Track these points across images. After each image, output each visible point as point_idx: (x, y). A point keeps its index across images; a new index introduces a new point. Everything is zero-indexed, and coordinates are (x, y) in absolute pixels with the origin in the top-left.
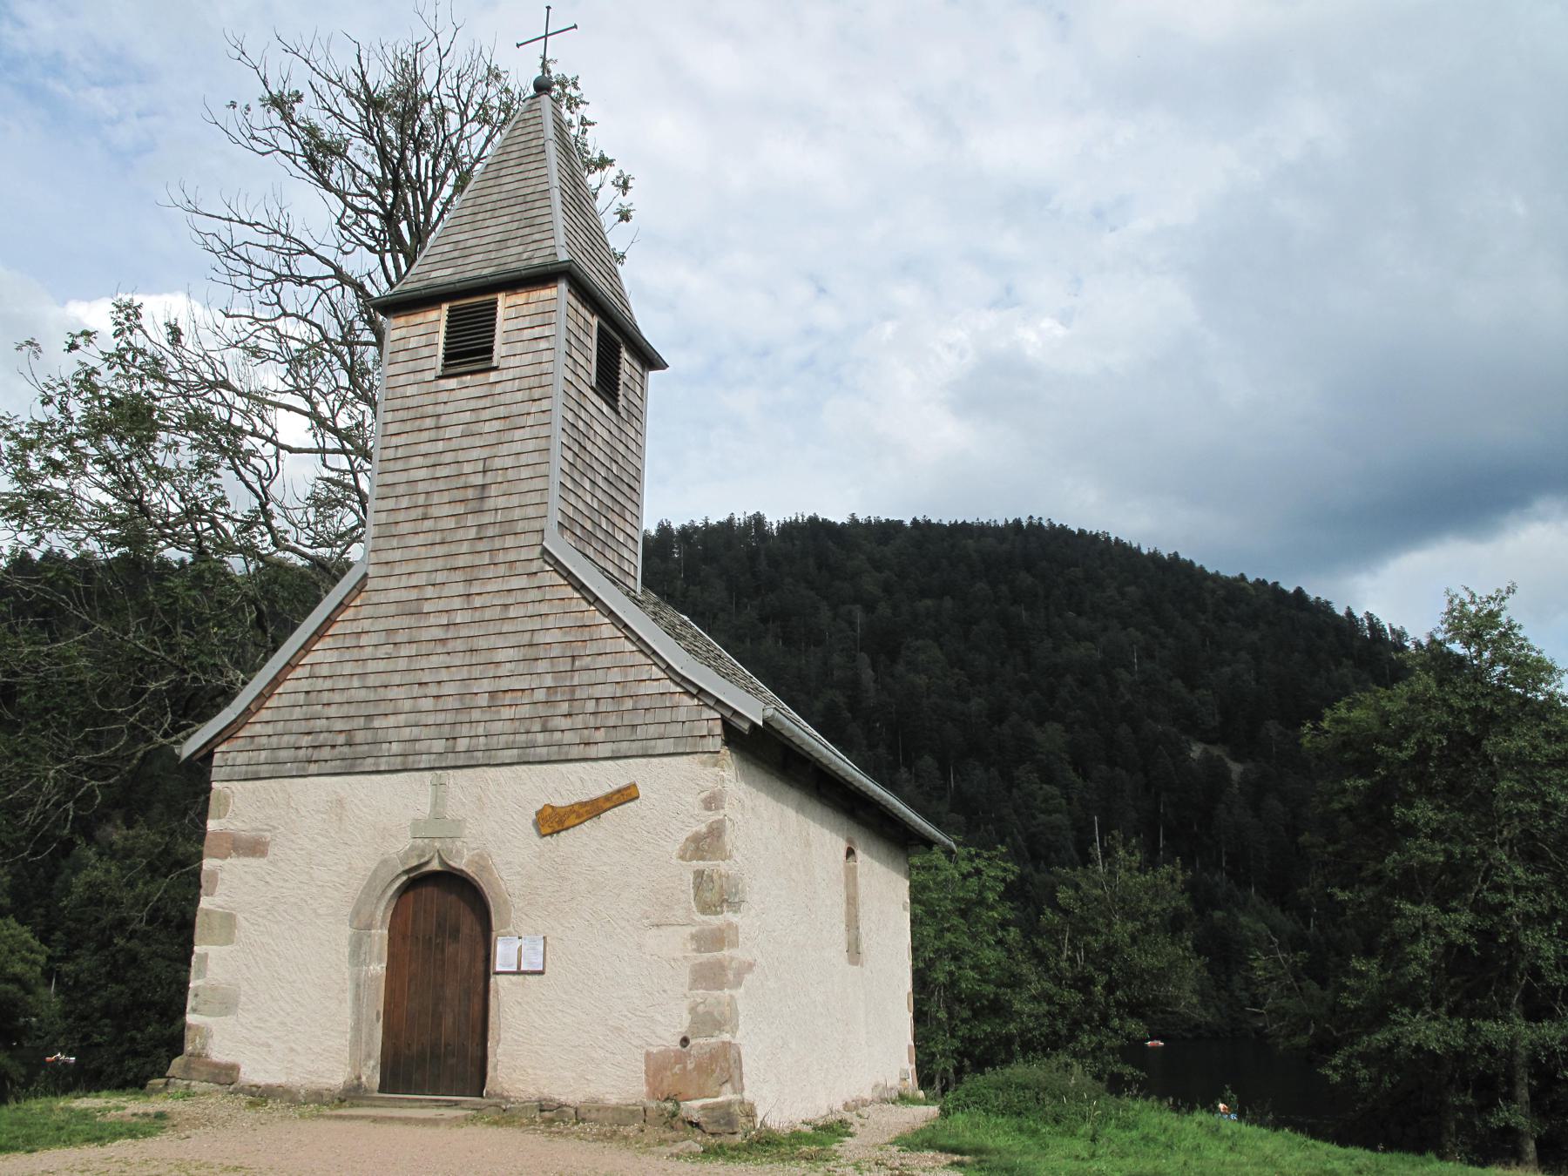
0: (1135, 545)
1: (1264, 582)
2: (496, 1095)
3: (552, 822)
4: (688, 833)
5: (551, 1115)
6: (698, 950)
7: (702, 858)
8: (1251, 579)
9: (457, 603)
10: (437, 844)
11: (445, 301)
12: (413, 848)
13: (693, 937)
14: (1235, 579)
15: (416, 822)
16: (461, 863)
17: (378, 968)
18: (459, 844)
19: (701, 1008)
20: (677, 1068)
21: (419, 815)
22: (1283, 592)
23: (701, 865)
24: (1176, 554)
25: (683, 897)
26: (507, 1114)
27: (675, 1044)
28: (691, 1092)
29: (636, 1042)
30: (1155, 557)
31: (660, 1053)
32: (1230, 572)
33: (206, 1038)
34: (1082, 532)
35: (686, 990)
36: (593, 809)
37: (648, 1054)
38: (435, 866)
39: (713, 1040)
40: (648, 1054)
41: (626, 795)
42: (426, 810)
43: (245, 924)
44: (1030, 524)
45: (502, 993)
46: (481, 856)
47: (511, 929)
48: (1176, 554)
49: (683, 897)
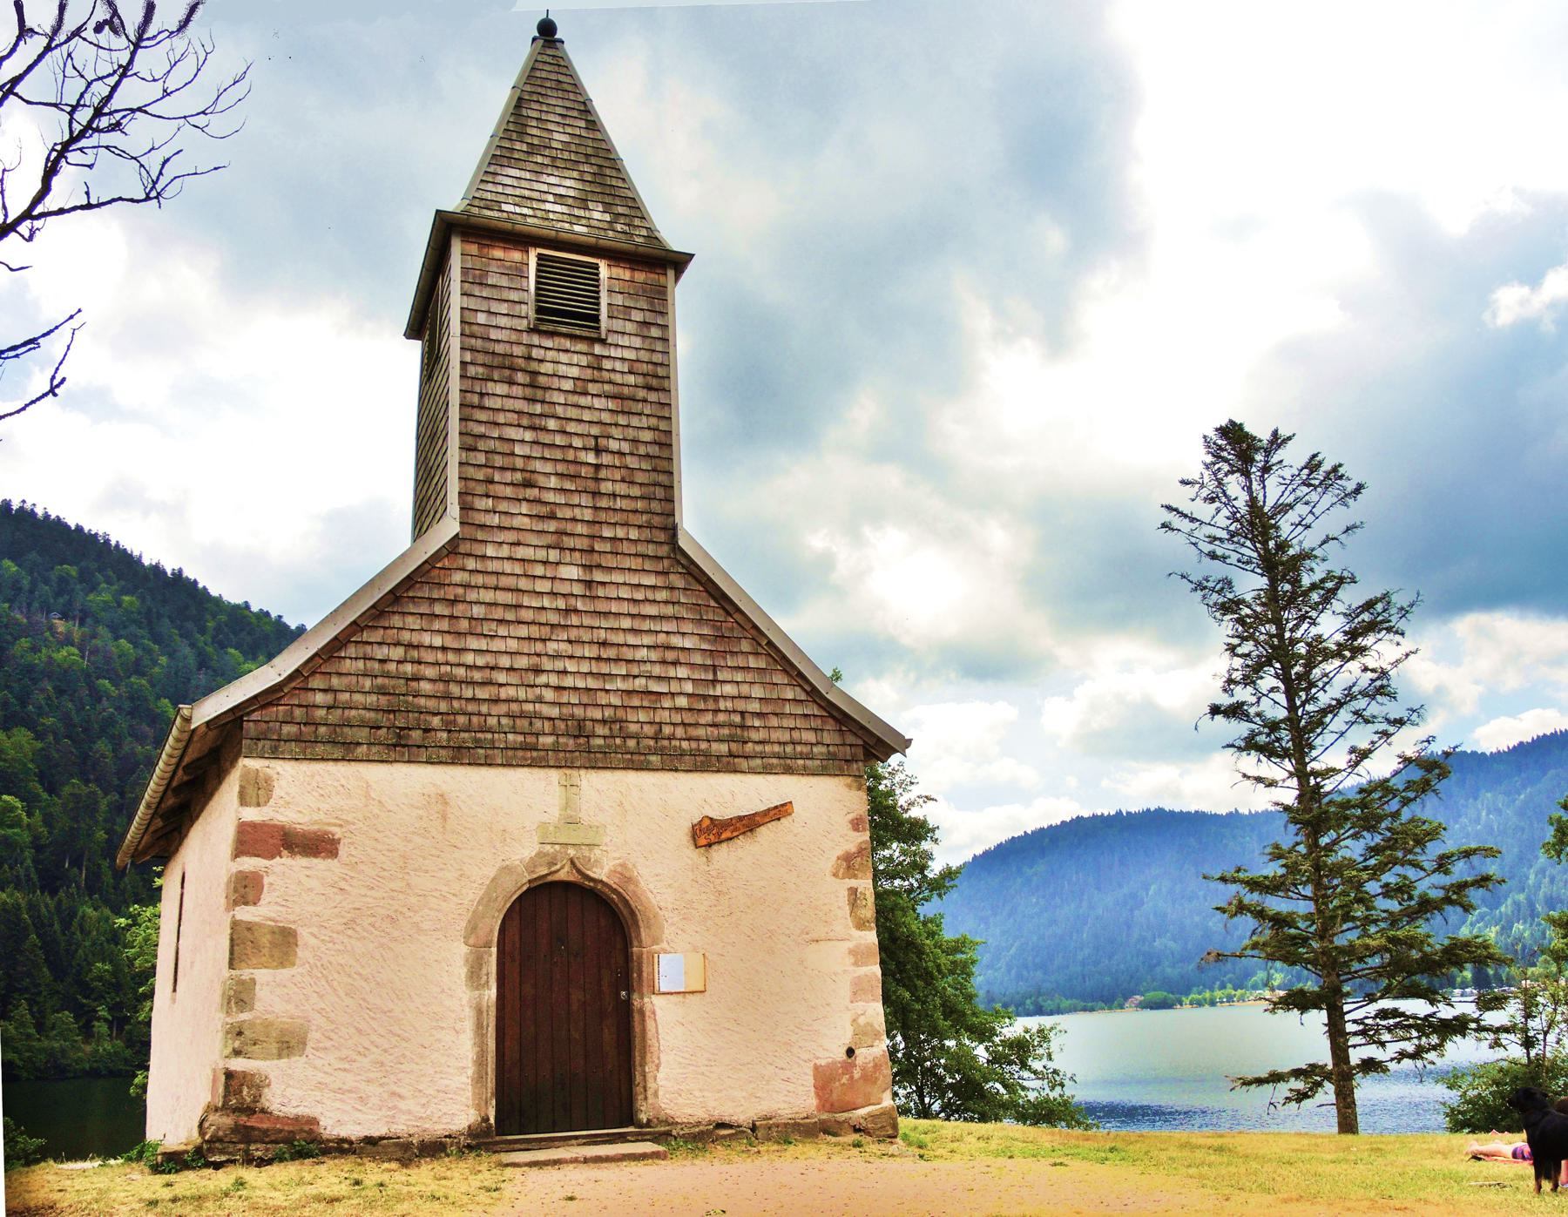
0: (136, 553)
1: (268, 614)
2: (660, 1122)
3: (712, 833)
4: (840, 852)
5: (710, 1135)
6: (856, 964)
7: (855, 877)
8: (255, 608)
9: (578, 589)
10: (571, 852)
11: (536, 245)
12: (539, 854)
13: (851, 952)
14: (237, 607)
15: (543, 826)
16: (602, 871)
17: (492, 993)
18: (597, 851)
19: (862, 1020)
20: (844, 1080)
21: (545, 818)
22: (286, 627)
23: (853, 883)
24: (180, 570)
25: (839, 913)
26: (673, 1138)
27: (841, 1055)
28: (860, 1101)
29: (806, 1056)
30: (157, 570)
31: (828, 1065)
32: (233, 596)
33: (259, 1087)
34: (79, 529)
35: (847, 1002)
36: (748, 824)
37: (816, 1068)
38: (564, 875)
39: (874, 1050)
40: (816, 1068)
41: (779, 812)
42: (554, 814)
43: (313, 941)
44: (21, 508)
45: (658, 1012)
46: (623, 865)
47: (664, 945)
48: (180, 570)
49: (839, 913)
